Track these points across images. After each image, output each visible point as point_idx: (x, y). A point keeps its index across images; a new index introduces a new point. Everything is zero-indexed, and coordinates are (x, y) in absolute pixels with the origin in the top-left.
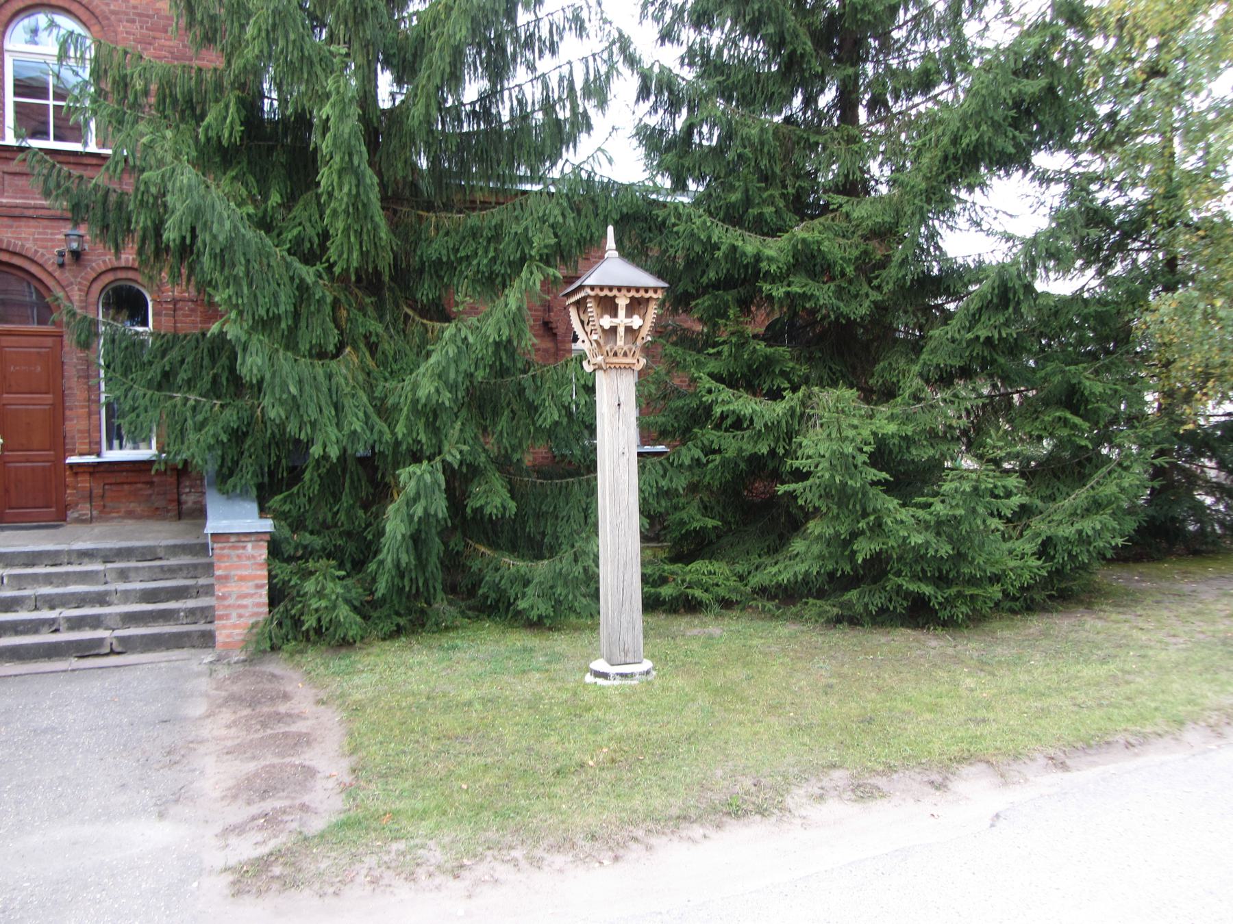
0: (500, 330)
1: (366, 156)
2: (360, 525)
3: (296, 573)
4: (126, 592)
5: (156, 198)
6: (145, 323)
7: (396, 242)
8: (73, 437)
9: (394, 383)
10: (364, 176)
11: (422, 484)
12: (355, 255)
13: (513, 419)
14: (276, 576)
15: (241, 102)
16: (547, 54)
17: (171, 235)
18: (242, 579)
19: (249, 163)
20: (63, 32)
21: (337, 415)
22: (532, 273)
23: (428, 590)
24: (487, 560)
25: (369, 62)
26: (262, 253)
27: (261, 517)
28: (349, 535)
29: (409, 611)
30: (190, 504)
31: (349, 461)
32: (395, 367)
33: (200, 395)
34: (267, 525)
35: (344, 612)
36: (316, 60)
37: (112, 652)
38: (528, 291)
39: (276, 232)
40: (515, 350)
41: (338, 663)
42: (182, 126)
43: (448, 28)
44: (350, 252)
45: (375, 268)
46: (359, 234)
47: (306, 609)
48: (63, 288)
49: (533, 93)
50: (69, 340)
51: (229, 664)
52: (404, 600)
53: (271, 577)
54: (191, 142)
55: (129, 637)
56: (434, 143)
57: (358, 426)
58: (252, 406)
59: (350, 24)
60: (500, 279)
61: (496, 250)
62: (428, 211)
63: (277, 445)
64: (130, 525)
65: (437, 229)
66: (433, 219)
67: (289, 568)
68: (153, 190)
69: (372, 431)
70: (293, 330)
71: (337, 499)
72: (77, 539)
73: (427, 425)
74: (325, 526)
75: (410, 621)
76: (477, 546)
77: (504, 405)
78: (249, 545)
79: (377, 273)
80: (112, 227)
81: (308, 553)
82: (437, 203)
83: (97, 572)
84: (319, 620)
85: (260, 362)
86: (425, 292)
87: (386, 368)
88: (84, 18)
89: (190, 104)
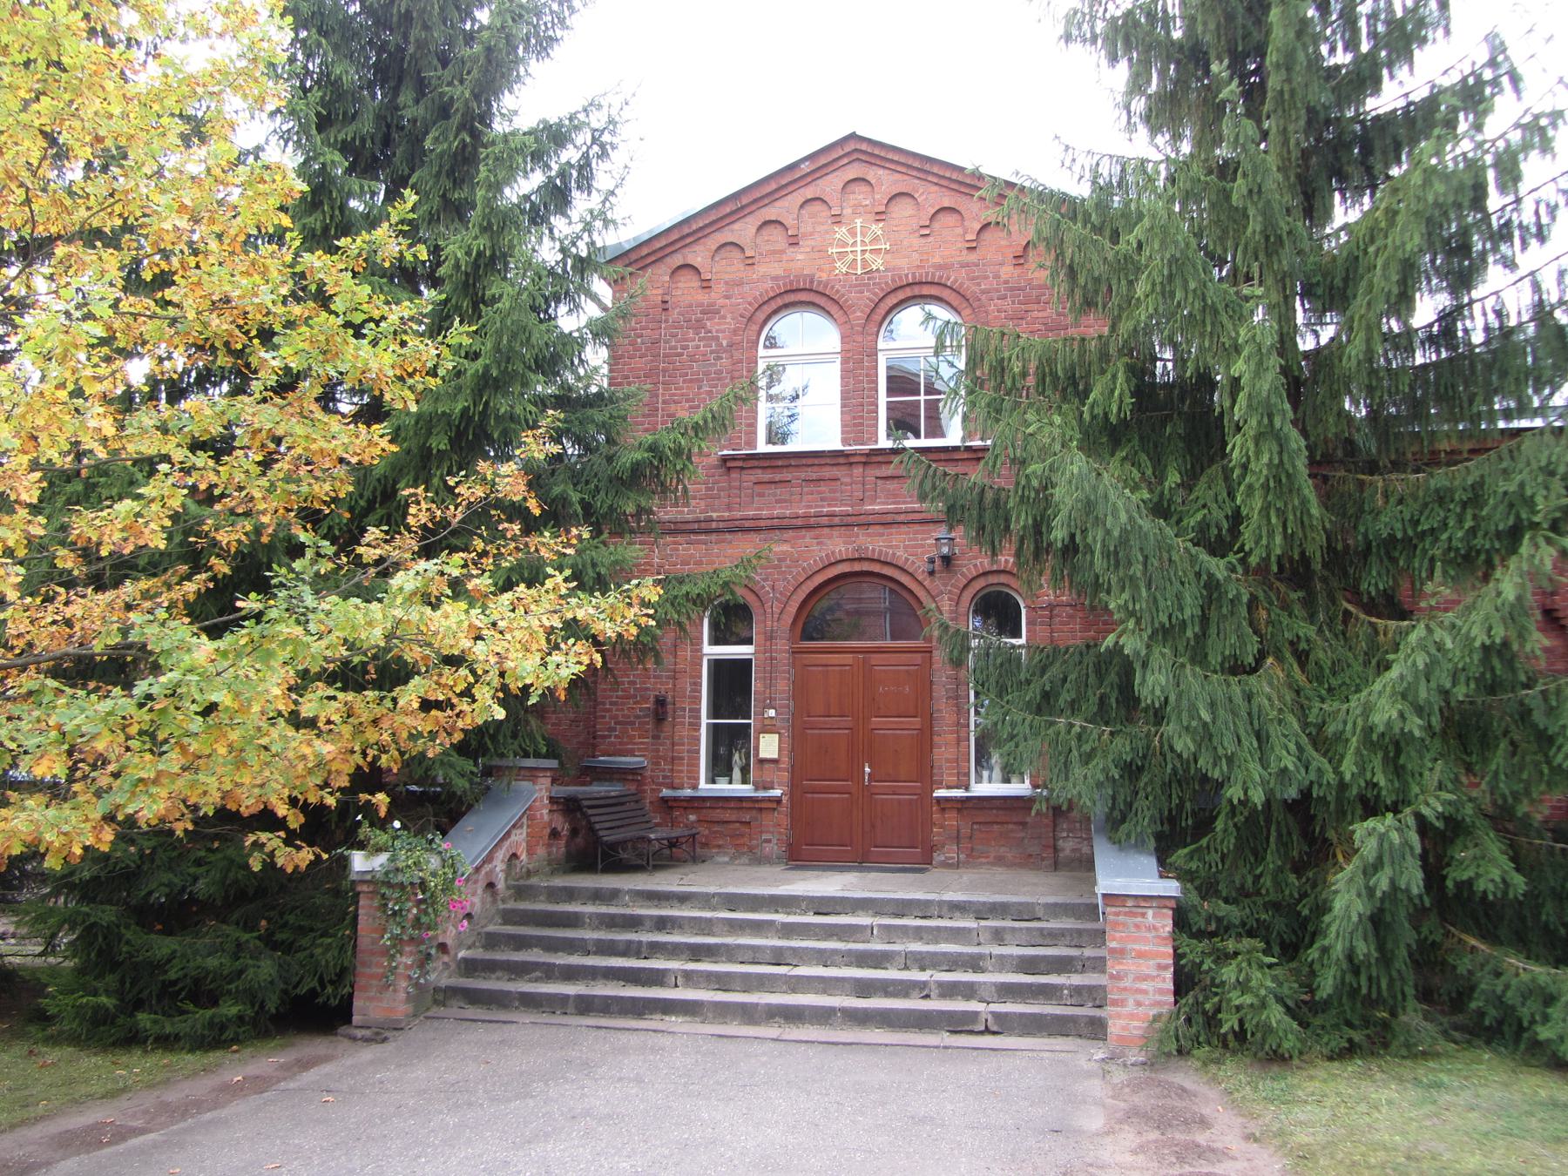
0: (1490, 629)
1: (1290, 415)
2: (1291, 895)
3: (1210, 954)
4: (1001, 957)
5: (1037, 492)
6: (1017, 635)
7: (1330, 520)
8: (940, 768)
9: (1336, 705)
10: (1287, 438)
11: (1386, 846)
12: (1278, 539)
13: (1514, 754)
14: (1183, 956)
15: (1132, 370)
16: (1534, 242)
17: (1059, 534)
18: (1141, 955)
19: (1141, 438)
20: (939, 323)
21: (1260, 747)
22: (1537, 546)
23: (1395, 997)
24: (1480, 959)
25: (1286, 297)
26: (1164, 547)
27: (1161, 877)
28: (1276, 906)
29: (1366, 1022)
30: (1067, 852)
31: (1274, 806)
32: (1335, 682)
33: (1086, 721)
34: (1171, 888)
35: (1276, 1015)
36: (1220, 307)
37: (988, 1031)
38: (1533, 575)
39: (1174, 519)
40: (1514, 656)
41: (1269, 1085)
42: (1065, 407)
43: (1395, 237)
44: (1271, 534)
45: (1303, 553)
46: (1281, 513)
47: (1224, 1004)
48: (933, 598)
49: (1518, 305)
50: (940, 656)
51: (1125, 1065)
52: (1359, 1005)
53: (1177, 956)
54: (1074, 423)
55: (1007, 1014)
56: (1374, 381)
57: (1289, 762)
58: (1148, 735)
59: (1262, 257)
60: (1483, 557)
61: (1475, 517)
62: (1372, 474)
63: (1179, 782)
64: (1000, 874)
65: (1386, 496)
66: (1380, 484)
67: (1204, 945)
68: (1035, 483)
69: (1307, 769)
70: (1202, 636)
71: (1259, 857)
72: (947, 888)
73: (1386, 759)
74: (1243, 893)
75: (1368, 1036)
76: (1464, 936)
77: (1499, 733)
78: (1150, 913)
79: (1305, 560)
80: (988, 529)
81: (1223, 928)
82: (1384, 462)
83: (969, 930)
84: (1241, 1022)
85: (1163, 680)
86: (1374, 581)
87: (1321, 683)
88: (955, 304)
89: (1072, 380)
